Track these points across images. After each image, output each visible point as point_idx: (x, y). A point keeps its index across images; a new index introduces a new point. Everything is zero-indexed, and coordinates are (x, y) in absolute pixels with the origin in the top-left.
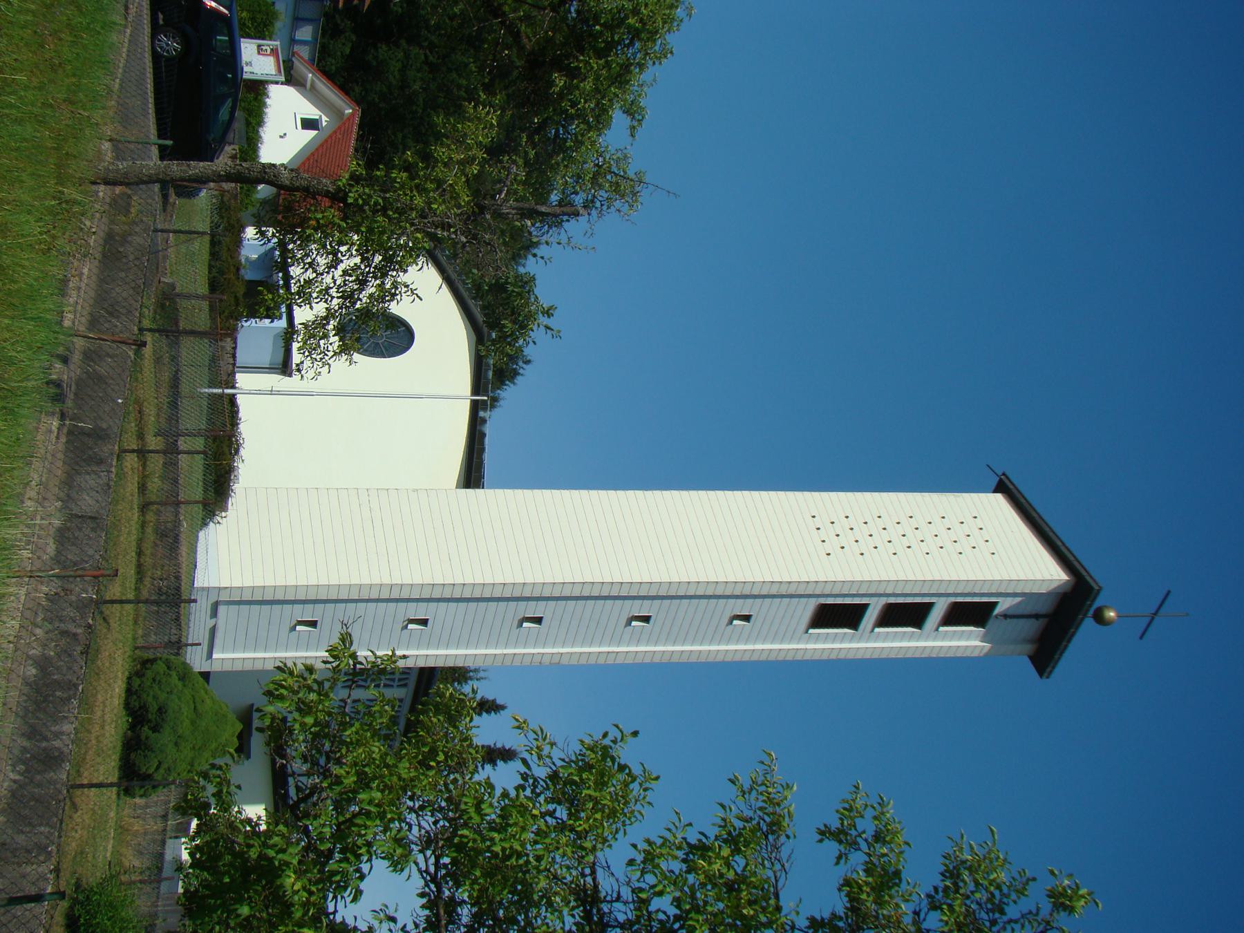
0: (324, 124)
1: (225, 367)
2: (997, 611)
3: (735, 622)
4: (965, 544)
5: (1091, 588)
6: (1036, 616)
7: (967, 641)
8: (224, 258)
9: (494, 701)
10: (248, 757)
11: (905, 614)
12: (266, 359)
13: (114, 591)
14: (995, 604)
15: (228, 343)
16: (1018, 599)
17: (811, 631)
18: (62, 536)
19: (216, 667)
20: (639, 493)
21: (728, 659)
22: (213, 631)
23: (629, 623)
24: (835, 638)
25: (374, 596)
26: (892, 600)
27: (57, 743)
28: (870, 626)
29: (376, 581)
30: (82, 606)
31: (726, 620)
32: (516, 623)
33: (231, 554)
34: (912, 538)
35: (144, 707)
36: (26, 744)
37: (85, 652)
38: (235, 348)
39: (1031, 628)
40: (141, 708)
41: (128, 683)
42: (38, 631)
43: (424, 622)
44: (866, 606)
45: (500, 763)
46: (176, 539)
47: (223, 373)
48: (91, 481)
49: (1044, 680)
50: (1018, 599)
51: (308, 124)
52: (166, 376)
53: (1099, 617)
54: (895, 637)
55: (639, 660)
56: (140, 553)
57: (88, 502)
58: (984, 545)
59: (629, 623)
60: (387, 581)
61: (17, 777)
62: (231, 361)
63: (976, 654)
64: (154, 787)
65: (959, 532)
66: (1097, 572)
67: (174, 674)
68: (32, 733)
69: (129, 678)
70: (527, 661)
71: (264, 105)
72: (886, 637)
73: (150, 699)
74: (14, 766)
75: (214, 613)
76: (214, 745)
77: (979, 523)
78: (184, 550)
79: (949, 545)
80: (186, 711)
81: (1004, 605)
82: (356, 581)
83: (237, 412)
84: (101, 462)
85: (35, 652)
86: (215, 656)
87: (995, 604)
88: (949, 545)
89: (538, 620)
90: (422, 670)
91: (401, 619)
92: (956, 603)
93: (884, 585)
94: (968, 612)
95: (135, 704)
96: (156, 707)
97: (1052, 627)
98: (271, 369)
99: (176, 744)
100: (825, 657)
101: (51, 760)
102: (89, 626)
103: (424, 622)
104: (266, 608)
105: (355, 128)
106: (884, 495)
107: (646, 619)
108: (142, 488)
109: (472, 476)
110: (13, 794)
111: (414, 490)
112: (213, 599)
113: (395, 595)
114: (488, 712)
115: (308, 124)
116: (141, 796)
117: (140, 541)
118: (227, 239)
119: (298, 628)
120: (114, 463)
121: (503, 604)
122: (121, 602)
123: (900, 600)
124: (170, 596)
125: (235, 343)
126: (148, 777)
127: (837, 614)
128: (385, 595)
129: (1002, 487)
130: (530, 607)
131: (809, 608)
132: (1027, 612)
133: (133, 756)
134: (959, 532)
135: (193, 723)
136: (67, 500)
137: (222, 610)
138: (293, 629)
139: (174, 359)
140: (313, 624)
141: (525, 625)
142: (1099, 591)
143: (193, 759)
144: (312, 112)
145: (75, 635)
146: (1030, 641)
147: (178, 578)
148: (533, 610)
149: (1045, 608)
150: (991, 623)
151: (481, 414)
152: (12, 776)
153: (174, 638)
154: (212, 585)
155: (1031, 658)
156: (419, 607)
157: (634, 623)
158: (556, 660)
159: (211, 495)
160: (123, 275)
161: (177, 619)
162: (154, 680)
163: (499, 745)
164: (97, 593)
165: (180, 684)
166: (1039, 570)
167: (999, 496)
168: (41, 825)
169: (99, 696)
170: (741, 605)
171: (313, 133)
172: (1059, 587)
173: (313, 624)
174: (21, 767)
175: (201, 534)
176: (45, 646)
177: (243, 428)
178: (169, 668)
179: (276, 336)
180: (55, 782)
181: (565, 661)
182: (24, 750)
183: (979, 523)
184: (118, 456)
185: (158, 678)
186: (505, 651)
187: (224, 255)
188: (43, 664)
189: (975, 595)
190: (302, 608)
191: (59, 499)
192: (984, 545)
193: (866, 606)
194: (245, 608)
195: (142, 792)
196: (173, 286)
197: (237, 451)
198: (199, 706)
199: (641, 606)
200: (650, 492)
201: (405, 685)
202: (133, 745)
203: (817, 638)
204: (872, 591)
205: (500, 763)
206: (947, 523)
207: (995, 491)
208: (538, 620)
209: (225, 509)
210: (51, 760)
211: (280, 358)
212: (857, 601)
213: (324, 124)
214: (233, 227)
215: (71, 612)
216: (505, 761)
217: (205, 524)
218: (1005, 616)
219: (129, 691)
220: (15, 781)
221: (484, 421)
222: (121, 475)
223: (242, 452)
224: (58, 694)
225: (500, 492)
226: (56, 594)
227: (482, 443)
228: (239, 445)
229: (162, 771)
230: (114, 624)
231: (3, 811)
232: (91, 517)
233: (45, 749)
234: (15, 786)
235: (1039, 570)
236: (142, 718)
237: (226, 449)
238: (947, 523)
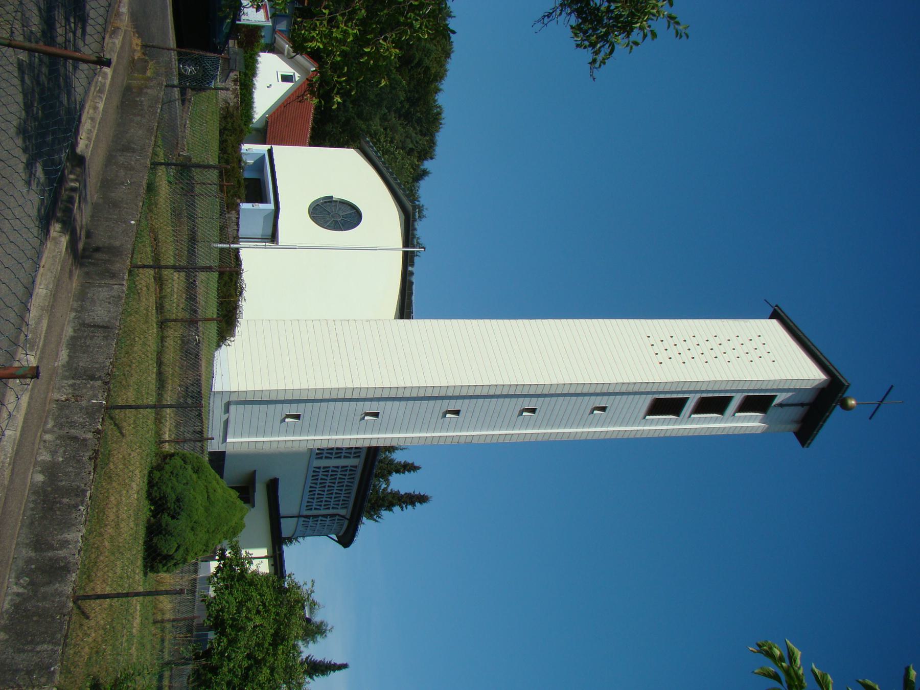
0: (297, 79)
1: (231, 231)
2: (776, 401)
3: (595, 412)
4: (754, 355)
5: (843, 385)
6: (802, 405)
7: (752, 422)
8: (229, 152)
9: (413, 464)
10: (253, 506)
11: (713, 404)
12: (258, 231)
13: (129, 396)
14: (775, 396)
15: (233, 215)
16: (790, 394)
17: (648, 417)
18: (75, 345)
19: (229, 449)
20: (526, 321)
21: (589, 438)
22: (226, 423)
23: (521, 413)
24: (664, 422)
25: (341, 396)
26: (705, 395)
27: (62, 553)
28: (688, 414)
29: (342, 386)
30: (91, 412)
31: (588, 411)
32: (441, 415)
33: (237, 367)
34: (718, 351)
35: (164, 498)
36: (33, 554)
37: (94, 458)
38: (238, 218)
39: (797, 413)
40: (160, 499)
41: (149, 476)
42: (48, 437)
43: (376, 415)
44: (686, 399)
45: (418, 504)
46: (197, 356)
47: (229, 232)
48: (103, 293)
49: (805, 449)
50: (790, 394)
51: (286, 78)
52: (185, 230)
53: (845, 406)
54: (705, 421)
55: (527, 440)
56: (160, 364)
57: (100, 313)
58: (764, 355)
59: (521, 413)
60: (350, 385)
61: (21, 590)
62: (236, 227)
63: (759, 431)
64: (175, 565)
65: (749, 346)
66: (846, 373)
67: (189, 467)
68: (39, 544)
69: (150, 473)
70: (448, 442)
71: (252, 98)
72: (699, 421)
73: (169, 490)
74: (18, 578)
75: (227, 410)
76: (225, 528)
77: (762, 340)
78: (203, 364)
79: (743, 355)
80: (200, 499)
81: (780, 398)
82: (327, 386)
83: (240, 265)
84: (113, 276)
85: (45, 457)
86: (228, 440)
87: (775, 396)
88: (743, 355)
89: (457, 412)
90: (369, 448)
91: (360, 412)
92: (748, 396)
93: (506, 389)
94: (756, 402)
95: (156, 494)
96: (174, 497)
97: (813, 412)
98: (263, 239)
99: (192, 529)
100: (656, 435)
101: (56, 570)
102: (98, 432)
103: (376, 415)
104: (264, 407)
105: (312, 111)
106: (696, 321)
107: (533, 411)
108: (160, 308)
109: (405, 310)
110: (16, 607)
111: (367, 321)
112: (226, 400)
113: (356, 396)
114: (409, 471)
115: (286, 78)
116: (165, 572)
117: (160, 354)
118: (232, 138)
119: (287, 420)
120: (126, 277)
121: (432, 402)
122: (137, 407)
123: (710, 395)
124: (194, 398)
125: (238, 214)
126: (168, 558)
127: (666, 405)
128: (348, 396)
129: (775, 315)
130: (450, 403)
131: (647, 401)
132: (796, 402)
133: (155, 540)
134: (749, 346)
135: (207, 510)
136: (81, 310)
137: (232, 408)
138: (283, 420)
139: (192, 217)
140: (297, 417)
141: (448, 416)
142: (848, 386)
143: (207, 542)
144: (288, 70)
145: (85, 440)
146: (797, 422)
147: (199, 386)
148: (453, 405)
149: (807, 399)
150: (771, 411)
151: (410, 269)
152: (16, 589)
153: (198, 429)
154: (225, 390)
155: (796, 434)
156: (371, 404)
157: (524, 414)
158: (469, 440)
159: (224, 325)
160: (139, 118)
161: (200, 415)
162: (172, 473)
163: (417, 493)
164: (107, 400)
165: (195, 476)
166: (805, 372)
167: (774, 321)
168: (43, 642)
169: (112, 499)
170: (599, 400)
171: (288, 85)
172: (816, 383)
173: (297, 417)
174: (25, 580)
175: (217, 354)
176: (54, 453)
177: (245, 276)
178: (185, 462)
179: (265, 217)
180: (60, 594)
181: (475, 441)
182: (29, 561)
183: (762, 340)
184: (130, 272)
185: (175, 472)
186: (434, 435)
187: (230, 150)
188: (51, 471)
189: (762, 390)
190: (292, 407)
191: (72, 310)
192: (764, 355)
193: (686, 399)
194: (249, 407)
195: (165, 568)
196: (190, 159)
197: (241, 293)
198: (211, 496)
199: (529, 401)
200: (533, 321)
201: (358, 457)
202: (154, 530)
203: (652, 423)
204: (691, 389)
205: (418, 504)
206: (740, 340)
207: (770, 318)
208: (457, 412)
209: (234, 336)
210: (56, 570)
211: (269, 231)
212: (680, 396)
213: (297, 79)
214: (235, 130)
215: (78, 418)
216: (421, 503)
217: (219, 346)
218: (781, 405)
219: (151, 484)
220: (18, 594)
221: (412, 274)
222: (133, 290)
223: (245, 294)
224: (66, 500)
225: (421, 321)
226: (67, 400)
227: (411, 289)
228: (242, 289)
229: (181, 551)
230: (128, 429)
231: (5, 629)
232: (103, 327)
233: (51, 559)
234: (18, 600)
235: (805, 372)
236: (163, 508)
237: (233, 292)
238: (740, 340)
